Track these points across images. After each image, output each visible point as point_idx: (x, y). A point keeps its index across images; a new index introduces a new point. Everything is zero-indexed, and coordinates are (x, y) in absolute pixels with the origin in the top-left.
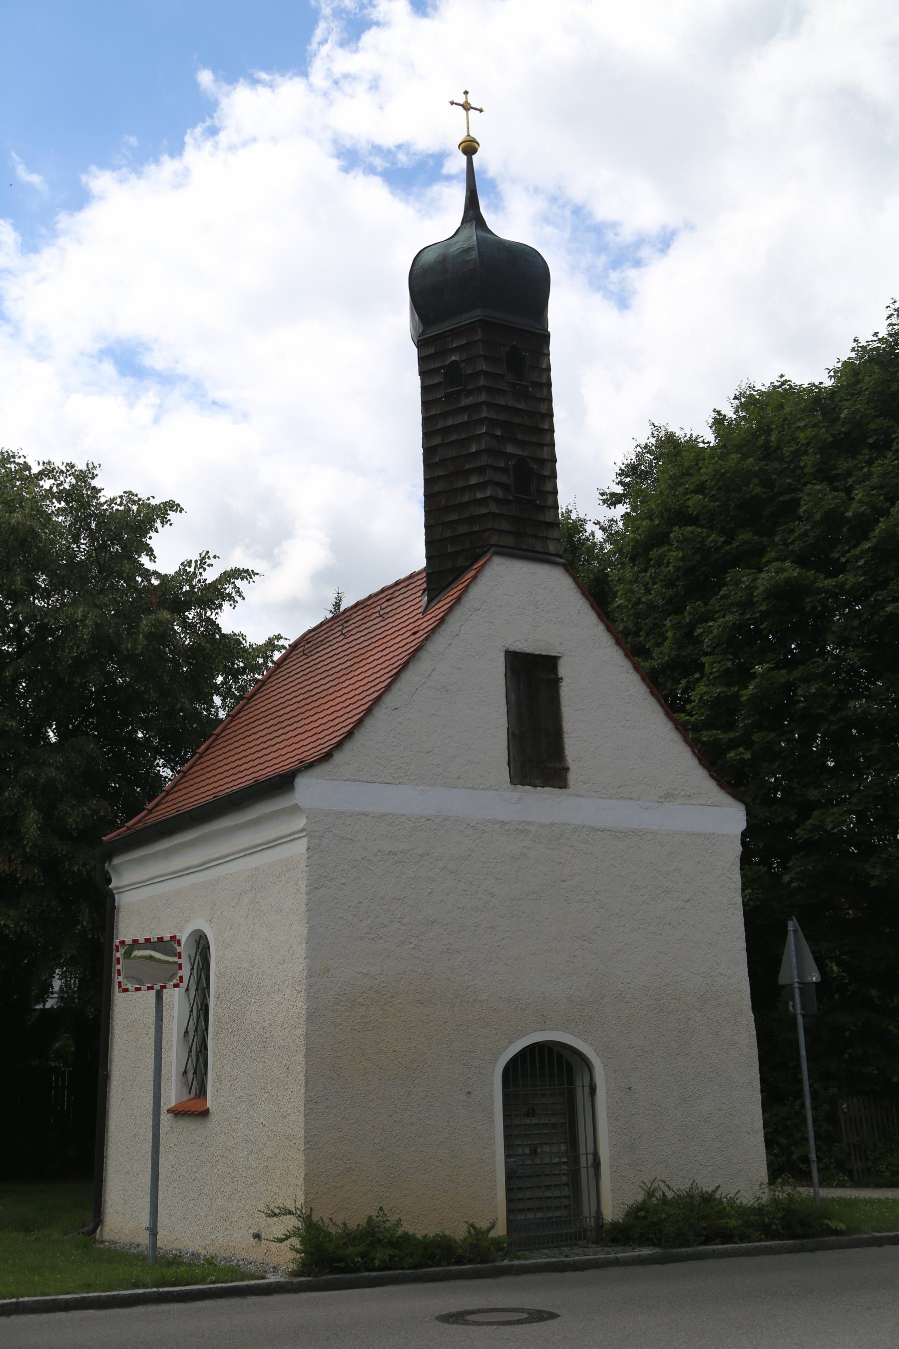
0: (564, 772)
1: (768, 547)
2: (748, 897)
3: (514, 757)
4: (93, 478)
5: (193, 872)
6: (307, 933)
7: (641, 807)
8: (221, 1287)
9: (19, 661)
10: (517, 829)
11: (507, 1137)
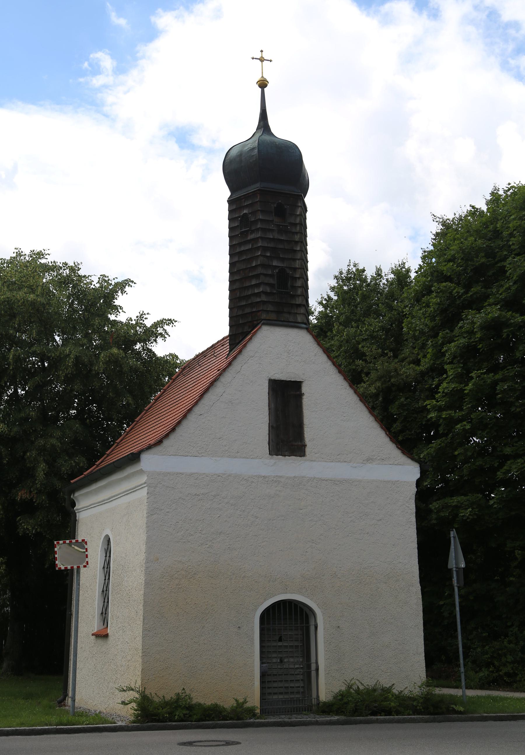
0: (304, 447)
1: (491, 295)
2: (469, 513)
3: (272, 440)
4: (78, 270)
5: (106, 503)
6: (146, 539)
8: (89, 727)
9: (36, 378)
10: (273, 480)
11: (262, 652)
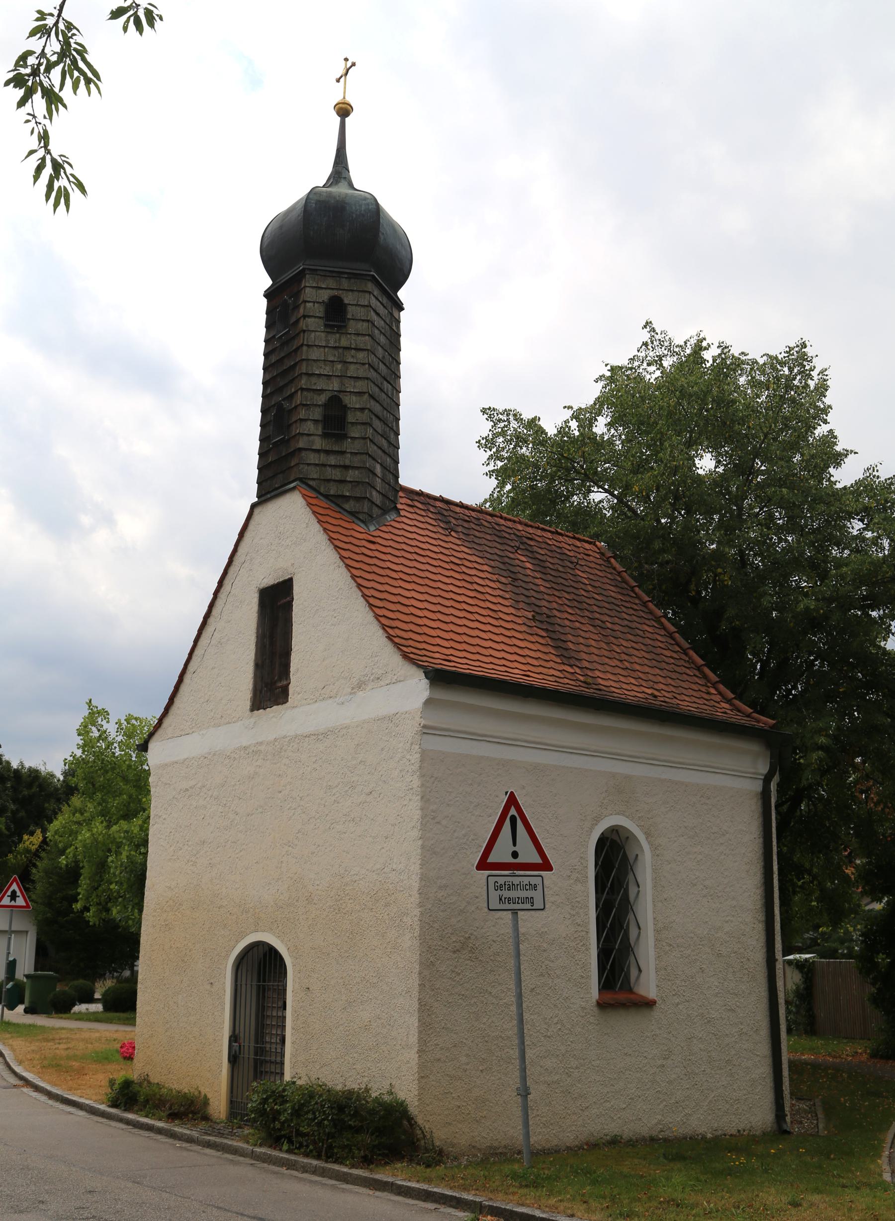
7: (338, 704)
